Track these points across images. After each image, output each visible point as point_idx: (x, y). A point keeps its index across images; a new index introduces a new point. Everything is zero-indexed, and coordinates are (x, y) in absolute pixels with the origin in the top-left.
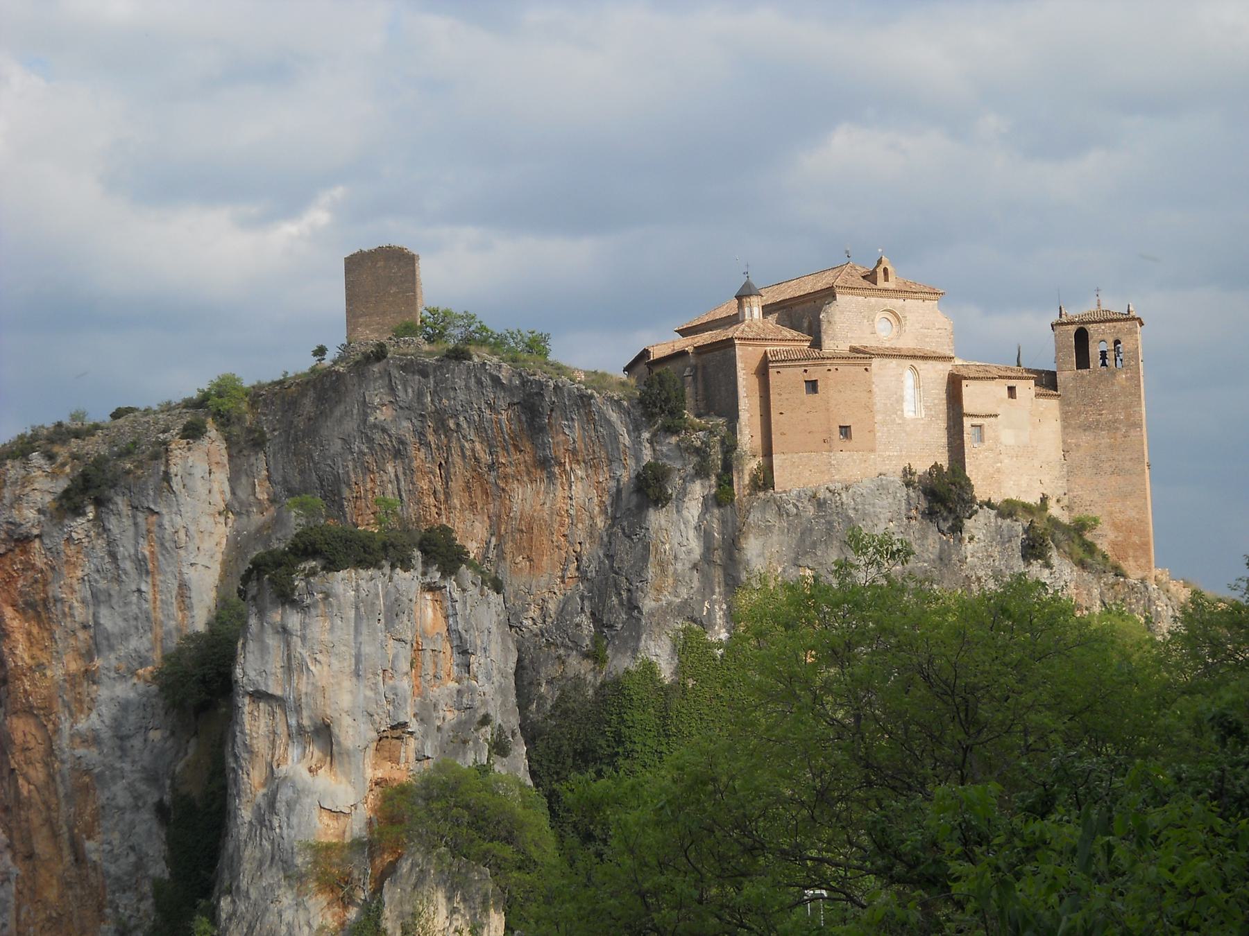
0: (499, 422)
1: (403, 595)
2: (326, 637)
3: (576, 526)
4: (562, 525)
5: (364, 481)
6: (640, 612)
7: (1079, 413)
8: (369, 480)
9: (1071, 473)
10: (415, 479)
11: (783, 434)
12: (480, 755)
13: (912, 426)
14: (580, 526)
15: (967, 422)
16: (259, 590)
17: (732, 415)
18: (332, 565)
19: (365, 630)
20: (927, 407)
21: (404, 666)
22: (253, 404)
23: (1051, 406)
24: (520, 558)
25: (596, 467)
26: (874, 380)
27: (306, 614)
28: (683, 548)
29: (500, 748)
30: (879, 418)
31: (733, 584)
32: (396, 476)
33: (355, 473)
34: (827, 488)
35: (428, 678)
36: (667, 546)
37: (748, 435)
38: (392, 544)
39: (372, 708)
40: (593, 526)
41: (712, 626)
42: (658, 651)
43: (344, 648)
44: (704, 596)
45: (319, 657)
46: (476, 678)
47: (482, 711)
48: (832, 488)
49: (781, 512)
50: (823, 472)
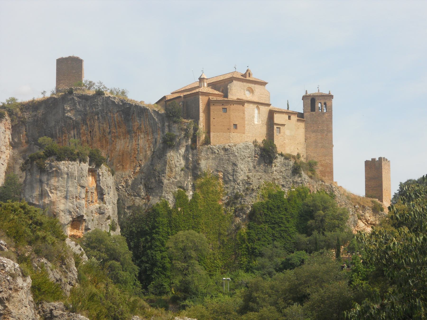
0: (114, 117)
1: (84, 171)
2: (56, 184)
3: (140, 154)
4: (135, 154)
5: (62, 136)
6: (163, 184)
7: (311, 127)
8: (64, 136)
9: (307, 147)
10: (81, 136)
11: (214, 126)
12: (107, 229)
13: (257, 126)
14: (141, 154)
15: (275, 127)
16: (31, 167)
17: (196, 119)
18: (59, 159)
19: (70, 183)
20: (262, 121)
21: (83, 196)
22: (21, 109)
23: (302, 125)
24: (119, 165)
25: (148, 134)
26: (245, 109)
27: (49, 175)
28: (179, 163)
29: (113, 228)
30: (246, 122)
31: (196, 177)
32: (74, 135)
33: (59, 133)
34: (229, 145)
35: (89, 202)
36: (173, 162)
37: (202, 125)
38: (81, 153)
39: (72, 210)
40: (146, 154)
41: (187, 190)
42: (169, 198)
43: (62, 188)
44: (185, 179)
45: (53, 191)
46: (105, 203)
47: (108, 215)
48: (230, 145)
49: (213, 153)
50: (227, 139)
